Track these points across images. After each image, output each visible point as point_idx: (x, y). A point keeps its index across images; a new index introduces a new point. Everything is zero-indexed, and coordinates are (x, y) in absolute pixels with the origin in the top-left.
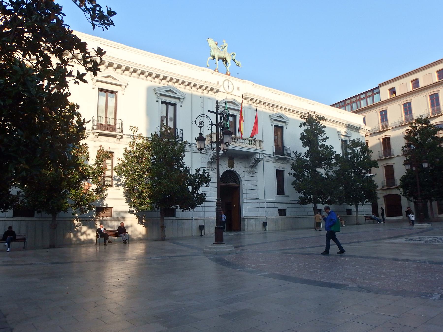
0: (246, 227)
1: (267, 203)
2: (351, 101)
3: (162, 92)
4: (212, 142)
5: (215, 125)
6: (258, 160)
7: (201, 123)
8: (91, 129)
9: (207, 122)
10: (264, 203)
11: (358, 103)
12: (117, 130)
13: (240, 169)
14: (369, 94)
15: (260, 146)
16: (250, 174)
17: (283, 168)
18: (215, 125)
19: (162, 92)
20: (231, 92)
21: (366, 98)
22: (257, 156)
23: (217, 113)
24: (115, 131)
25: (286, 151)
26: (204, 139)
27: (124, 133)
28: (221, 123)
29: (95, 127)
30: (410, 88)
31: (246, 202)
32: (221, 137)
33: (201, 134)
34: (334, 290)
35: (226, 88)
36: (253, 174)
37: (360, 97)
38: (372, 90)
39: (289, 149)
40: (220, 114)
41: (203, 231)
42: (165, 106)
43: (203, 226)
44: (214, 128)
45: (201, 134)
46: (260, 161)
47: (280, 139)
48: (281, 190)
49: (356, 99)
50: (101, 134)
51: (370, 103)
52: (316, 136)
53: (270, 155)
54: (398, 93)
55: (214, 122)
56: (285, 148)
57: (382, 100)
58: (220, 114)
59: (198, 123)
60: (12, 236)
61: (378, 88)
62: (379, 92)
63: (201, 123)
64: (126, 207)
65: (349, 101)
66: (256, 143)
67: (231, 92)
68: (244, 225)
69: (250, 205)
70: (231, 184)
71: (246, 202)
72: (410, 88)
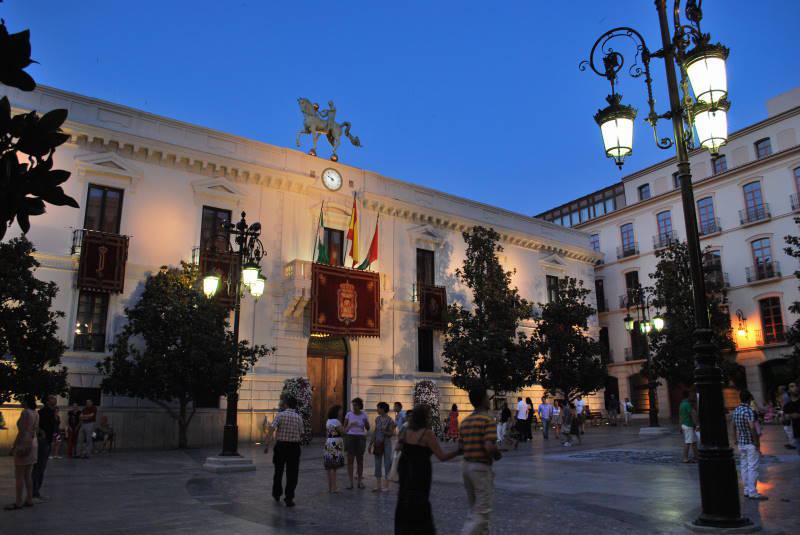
2: (570, 208)
5: (659, 54)
7: (611, 61)
11: (592, 208)
14: (584, 203)
18: (659, 54)
21: (604, 200)
28: (679, 36)
30: (752, 157)
34: (227, 193)
37: (593, 199)
38: (612, 188)
51: (585, 218)
54: (775, 149)
55: (655, 44)
57: (628, 204)
60: (47, 367)
61: (621, 184)
62: (623, 193)
63: (611, 61)
64: (653, 283)
72: (752, 157)
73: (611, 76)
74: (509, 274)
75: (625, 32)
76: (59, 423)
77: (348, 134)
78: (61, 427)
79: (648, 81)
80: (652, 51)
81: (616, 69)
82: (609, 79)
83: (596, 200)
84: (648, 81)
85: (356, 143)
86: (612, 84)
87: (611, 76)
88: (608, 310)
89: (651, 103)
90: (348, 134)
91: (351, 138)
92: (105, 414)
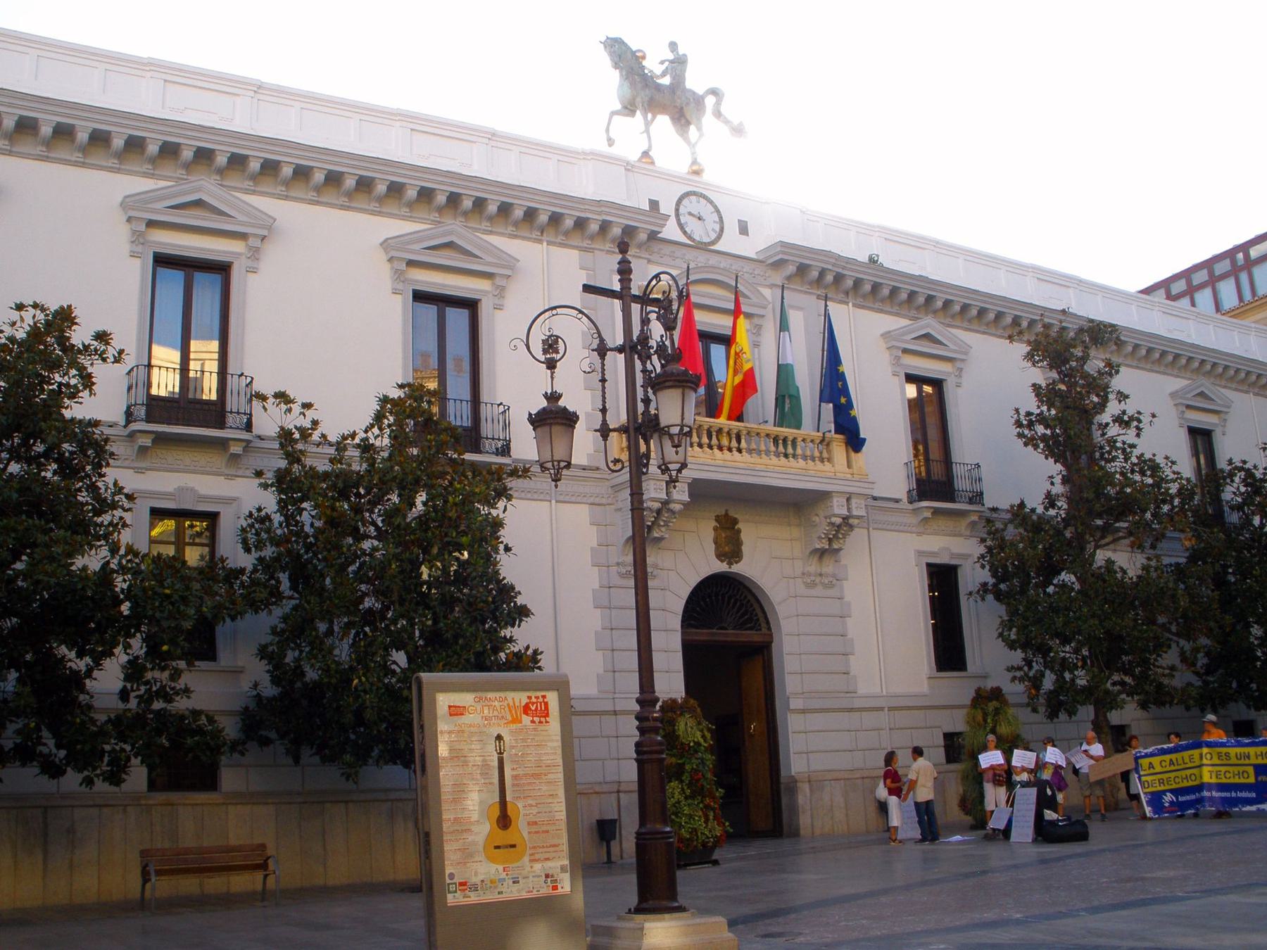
0: (804, 821)
1: (890, 709)
2: (1189, 282)
3: (906, 342)
4: (604, 431)
5: (620, 350)
6: (845, 525)
7: (551, 344)
8: (121, 420)
9: (573, 332)
10: (882, 709)
11: (1244, 277)
12: (230, 419)
13: (768, 560)
15: (849, 466)
16: (812, 585)
17: (953, 556)
18: (620, 350)
19: (906, 342)
20: (713, 243)
22: (838, 507)
23: (624, 295)
24: (221, 425)
25: (961, 484)
26: (569, 419)
27: (256, 431)
29: (142, 412)
31: (803, 711)
32: (647, 401)
33: (553, 397)
35: (692, 226)
36: (826, 586)
37: (1247, 256)
39: (975, 473)
40: (636, 299)
41: (614, 845)
42: (431, 310)
43: (613, 822)
44: (617, 362)
45: (553, 397)
46: (851, 527)
47: (933, 433)
48: (949, 651)
49: (1234, 262)
50: (161, 440)
52: (1087, 415)
53: (897, 501)
56: (958, 471)
58: (636, 299)
59: (537, 349)
63: (551, 344)
65: (1205, 272)
66: (829, 452)
67: (713, 243)
68: (794, 809)
69: (817, 721)
70: (731, 635)
71: (803, 711)
73: (551, 365)
74: (442, 732)
75: (654, 282)
76: (1178, 564)
77: (718, 114)
78: (124, 658)
79: (603, 380)
80: (610, 344)
81: (559, 356)
82: (548, 368)
83: (1205, 272)
84: (603, 380)
85: (738, 130)
86: (552, 374)
87: (551, 365)
88: (795, 834)
89: (604, 411)
90: (718, 114)
91: (727, 122)
92: (1174, 645)
